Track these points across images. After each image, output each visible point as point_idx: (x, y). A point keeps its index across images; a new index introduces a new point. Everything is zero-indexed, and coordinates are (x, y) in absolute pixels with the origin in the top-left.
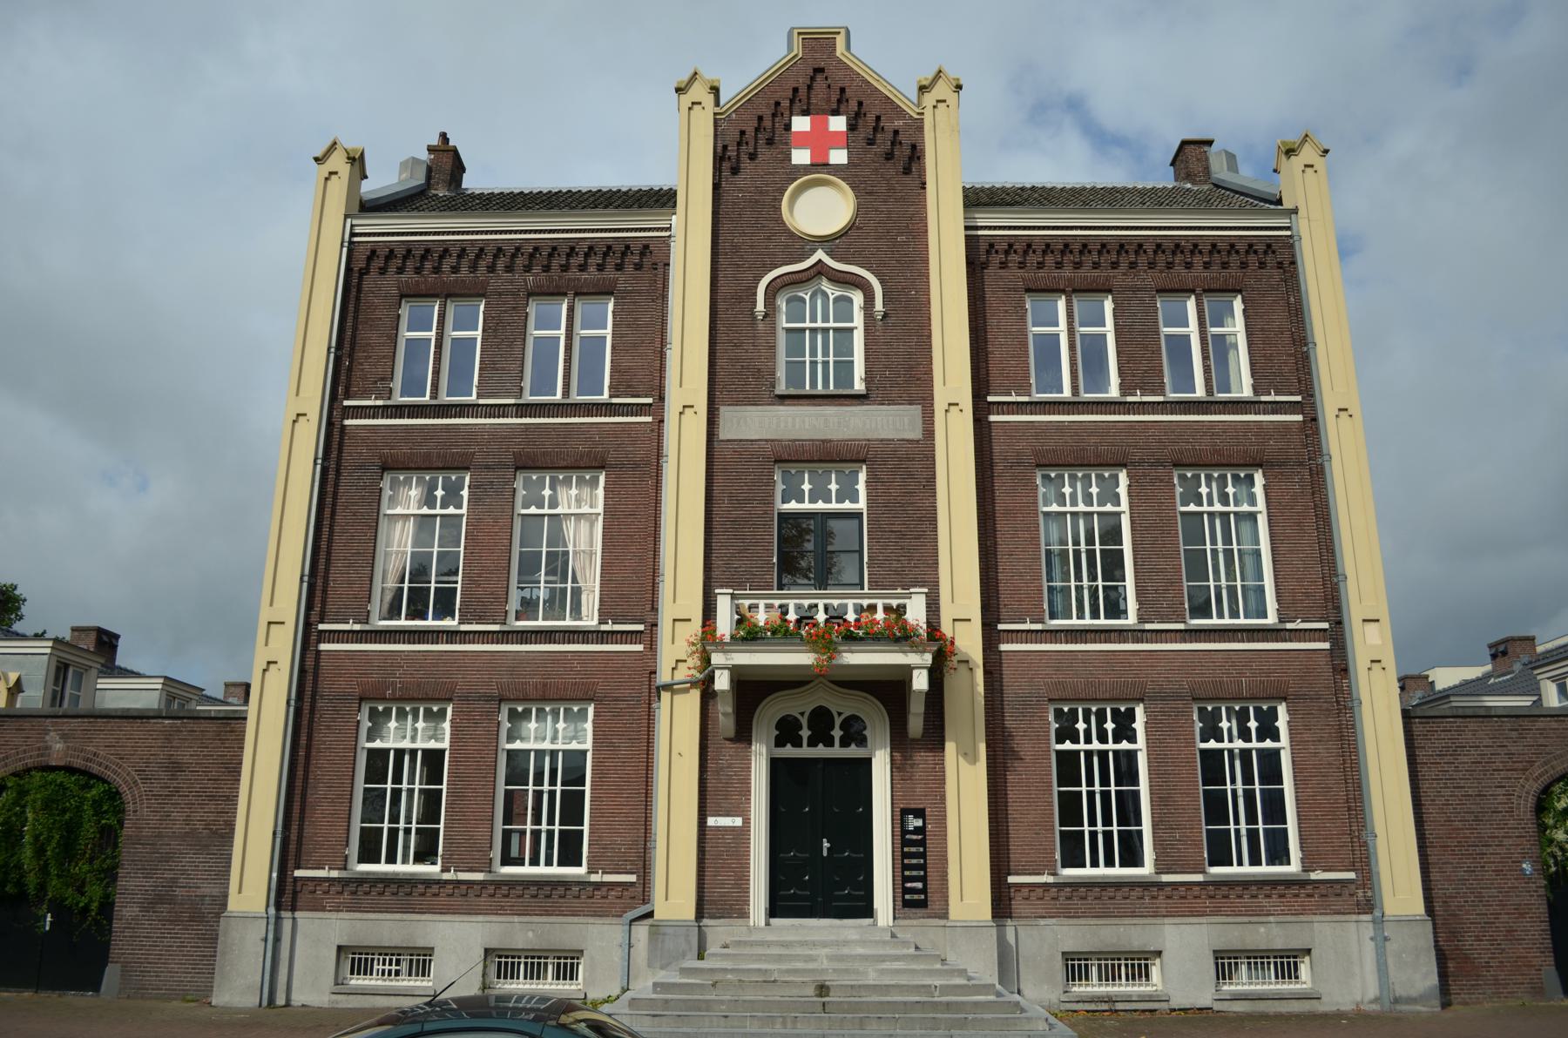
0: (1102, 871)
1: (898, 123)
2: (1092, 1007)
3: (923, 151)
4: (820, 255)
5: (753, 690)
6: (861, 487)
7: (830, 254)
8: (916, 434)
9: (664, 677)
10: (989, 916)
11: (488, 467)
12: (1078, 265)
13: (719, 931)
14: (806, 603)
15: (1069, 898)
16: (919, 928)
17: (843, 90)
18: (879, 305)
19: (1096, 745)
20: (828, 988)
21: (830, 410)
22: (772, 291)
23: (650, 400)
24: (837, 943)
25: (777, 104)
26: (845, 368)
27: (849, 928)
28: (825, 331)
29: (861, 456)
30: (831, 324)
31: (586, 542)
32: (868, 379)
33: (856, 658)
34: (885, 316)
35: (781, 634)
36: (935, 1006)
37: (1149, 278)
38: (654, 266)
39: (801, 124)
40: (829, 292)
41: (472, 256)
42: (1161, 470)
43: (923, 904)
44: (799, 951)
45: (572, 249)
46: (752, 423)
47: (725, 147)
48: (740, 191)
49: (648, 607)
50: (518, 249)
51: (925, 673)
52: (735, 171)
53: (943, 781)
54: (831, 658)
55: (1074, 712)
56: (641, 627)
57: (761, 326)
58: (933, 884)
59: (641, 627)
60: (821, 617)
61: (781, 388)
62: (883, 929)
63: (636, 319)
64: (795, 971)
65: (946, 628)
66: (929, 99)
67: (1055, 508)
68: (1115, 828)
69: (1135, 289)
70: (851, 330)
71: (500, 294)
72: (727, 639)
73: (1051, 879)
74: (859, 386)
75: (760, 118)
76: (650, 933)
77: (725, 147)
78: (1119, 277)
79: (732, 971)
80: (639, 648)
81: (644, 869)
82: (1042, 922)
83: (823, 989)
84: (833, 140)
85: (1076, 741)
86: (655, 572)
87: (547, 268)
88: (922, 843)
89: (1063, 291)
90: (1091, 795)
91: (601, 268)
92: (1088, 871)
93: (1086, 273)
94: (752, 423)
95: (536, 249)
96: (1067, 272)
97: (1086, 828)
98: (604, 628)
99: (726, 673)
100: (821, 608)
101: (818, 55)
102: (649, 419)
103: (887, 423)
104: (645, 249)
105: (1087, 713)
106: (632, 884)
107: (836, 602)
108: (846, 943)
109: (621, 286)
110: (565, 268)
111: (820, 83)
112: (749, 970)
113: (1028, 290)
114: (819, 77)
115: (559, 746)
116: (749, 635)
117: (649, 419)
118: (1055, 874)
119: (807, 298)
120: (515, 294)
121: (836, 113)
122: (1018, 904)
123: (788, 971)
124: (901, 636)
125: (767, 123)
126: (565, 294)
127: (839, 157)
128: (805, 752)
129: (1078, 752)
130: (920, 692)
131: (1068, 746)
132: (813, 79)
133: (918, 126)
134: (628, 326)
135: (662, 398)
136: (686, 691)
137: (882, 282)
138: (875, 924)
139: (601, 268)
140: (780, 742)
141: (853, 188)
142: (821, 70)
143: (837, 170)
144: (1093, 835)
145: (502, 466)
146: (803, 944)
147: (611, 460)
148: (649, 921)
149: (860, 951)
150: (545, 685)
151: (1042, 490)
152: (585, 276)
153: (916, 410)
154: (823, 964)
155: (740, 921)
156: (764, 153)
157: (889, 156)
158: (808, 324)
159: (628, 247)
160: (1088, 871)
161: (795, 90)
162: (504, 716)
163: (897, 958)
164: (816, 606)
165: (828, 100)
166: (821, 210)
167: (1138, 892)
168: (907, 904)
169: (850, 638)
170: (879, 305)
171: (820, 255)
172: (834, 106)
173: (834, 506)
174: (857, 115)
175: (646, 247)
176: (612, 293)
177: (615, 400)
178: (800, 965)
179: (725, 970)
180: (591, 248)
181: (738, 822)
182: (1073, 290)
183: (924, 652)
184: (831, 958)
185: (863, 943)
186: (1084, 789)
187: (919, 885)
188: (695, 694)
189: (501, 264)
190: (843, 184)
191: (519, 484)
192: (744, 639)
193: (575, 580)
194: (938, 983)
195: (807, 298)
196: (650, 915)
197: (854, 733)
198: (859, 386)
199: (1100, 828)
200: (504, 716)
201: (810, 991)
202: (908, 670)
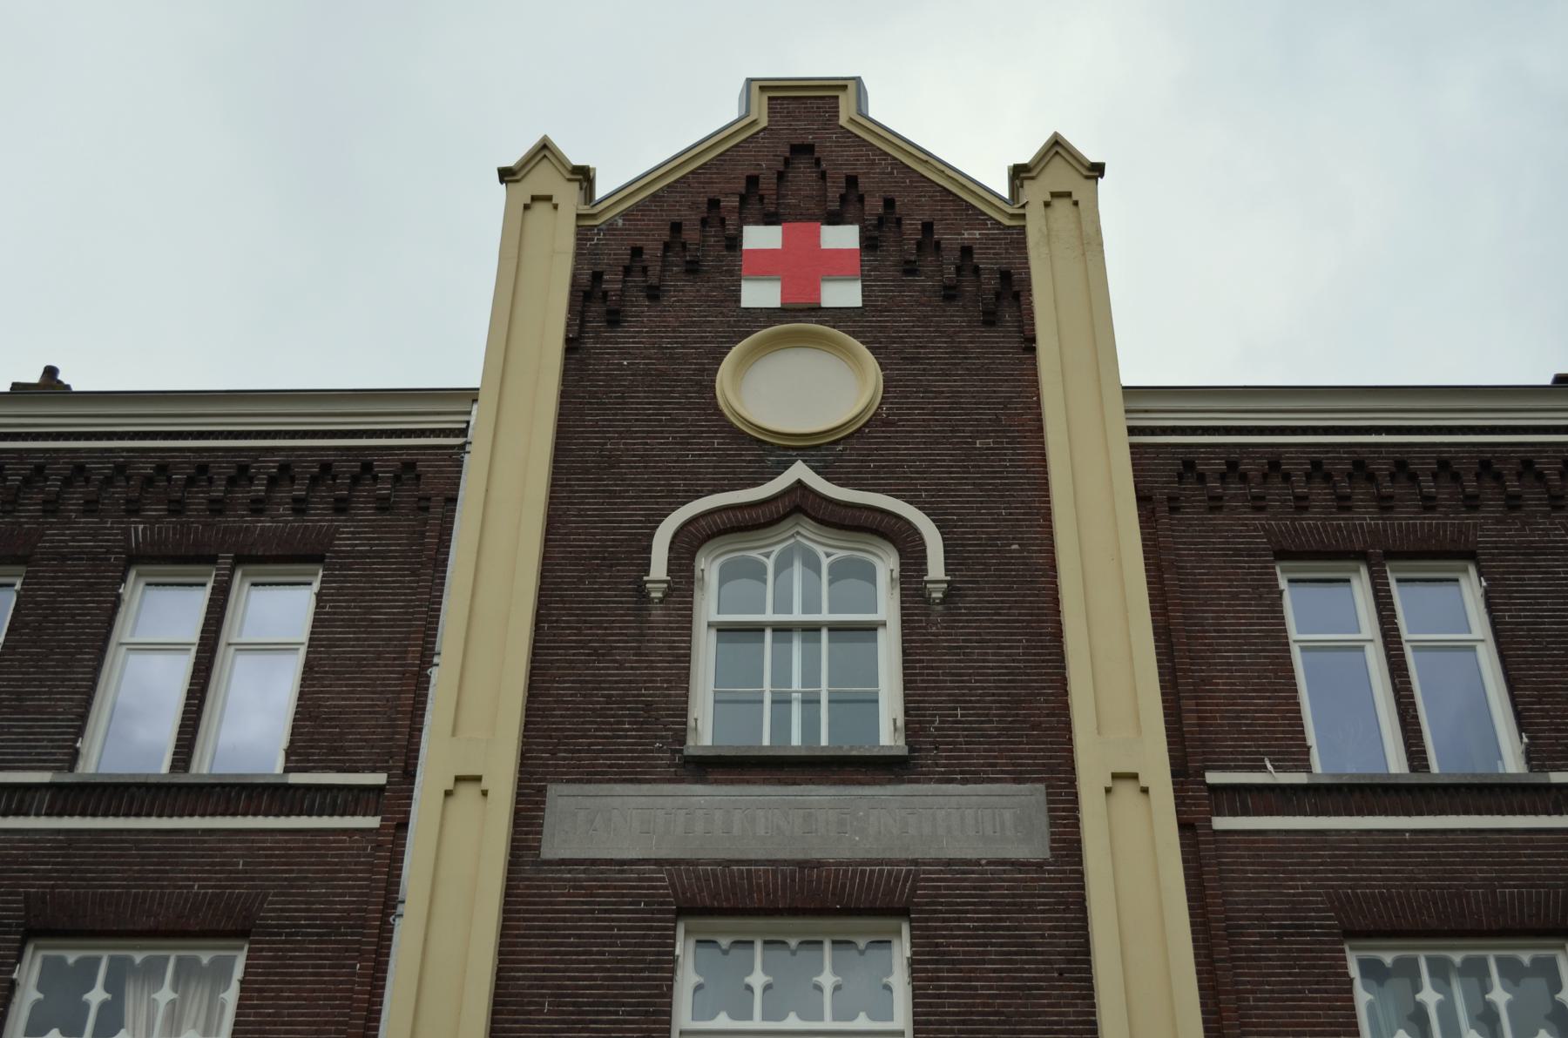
1: (971, 235)
3: (1027, 283)
4: (799, 471)
8: (1035, 847)
17: (852, 181)
18: (936, 567)
21: (820, 795)
22: (687, 544)
23: (380, 779)
28: (811, 629)
30: (825, 616)
32: (914, 722)
34: (951, 593)
39: (760, 238)
40: (820, 551)
47: (597, 277)
48: (625, 353)
52: (614, 319)
53: (427, 656)
57: (657, 614)
61: (704, 734)
66: (1034, 193)
70: (871, 629)
74: (888, 736)
89: (1362, 556)
102: (373, 822)
104: (408, 468)
109: (343, 543)
110: (217, 507)
111: (803, 173)
113: (1283, 555)
114: (802, 165)
117: (373, 822)
119: (770, 564)
121: (835, 219)
126: (211, 560)
133: (1017, 239)
137: (941, 526)
139: (300, 507)
141: (873, 351)
142: (808, 149)
143: (839, 317)
151: (1362, 997)
153: (1032, 796)
157: (950, 294)
158: (769, 616)
161: (752, 181)
165: (823, 198)
170: (936, 567)
171: (799, 471)
175: (409, 466)
176: (317, 559)
191: (29, 975)
195: (770, 564)
198: (888, 736)
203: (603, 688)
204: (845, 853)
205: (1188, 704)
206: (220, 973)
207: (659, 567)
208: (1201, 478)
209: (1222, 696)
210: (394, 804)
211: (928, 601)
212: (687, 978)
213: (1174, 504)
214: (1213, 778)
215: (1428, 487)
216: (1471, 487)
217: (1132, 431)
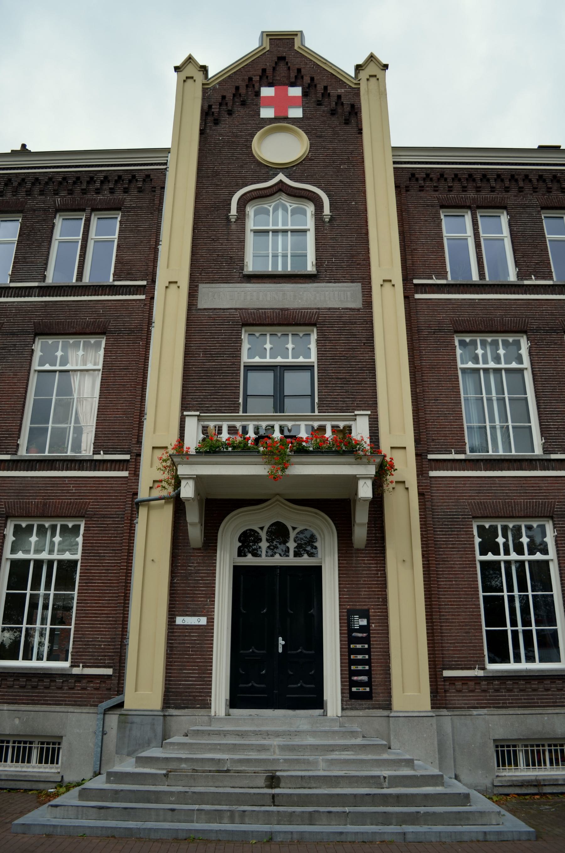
0: (524, 666)
1: (341, 91)
2: (524, 791)
4: (281, 177)
5: (218, 505)
6: (313, 347)
7: (289, 177)
8: (357, 304)
9: (143, 494)
10: (428, 707)
11: (13, 334)
12: (478, 190)
13: (184, 719)
14: (264, 424)
15: (497, 690)
16: (366, 719)
17: (299, 70)
19: (514, 556)
20: (278, 778)
21: (288, 287)
23: (144, 283)
24: (289, 734)
25: (250, 79)
26: (301, 257)
27: (301, 719)
29: (313, 321)
31: (87, 394)
33: (304, 469)
34: (332, 219)
35: (241, 450)
36: (386, 799)
37: (534, 199)
38: (153, 190)
39: (267, 92)
40: (288, 204)
41: (15, 184)
42: (554, 335)
43: (367, 696)
44: (254, 741)
45: (92, 178)
46: (223, 296)
47: (210, 107)
48: (221, 135)
49: (134, 441)
50: (50, 179)
51: (369, 483)
52: (216, 122)
54: (283, 469)
55: (494, 529)
56: (127, 457)
57: (233, 227)
58: (377, 678)
59: (127, 457)
60: (277, 435)
62: (332, 720)
63: (137, 226)
64: (248, 761)
65: (385, 448)
66: (363, 75)
67: (470, 365)
68: (534, 628)
69: (525, 207)
70: (305, 231)
71: (34, 210)
72: (192, 451)
73: (480, 673)
74: (310, 268)
75: (237, 88)
76: (119, 722)
77: (210, 107)
78: (511, 198)
79: (186, 760)
80: (125, 474)
81: (119, 662)
82: (475, 712)
83: (273, 781)
84: (293, 102)
85: (497, 553)
86: (142, 413)
87: (71, 192)
88: (367, 640)
89: (469, 207)
90: (511, 599)
91: (112, 191)
92: (511, 666)
93: (485, 195)
94: (223, 296)
95: (64, 179)
96: (471, 194)
97: (509, 628)
98: (97, 457)
99: (191, 483)
100: (277, 429)
101: (281, 49)
102: (143, 297)
103: (336, 296)
104: (148, 177)
105: (505, 529)
106: (109, 676)
107: (290, 424)
108: (297, 733)
109: (127, 204)
112: (202, 760)
113: (443, 207)
115: (55, 556)
116: (211, 449)
117: (143, 297)
118: (484, 669)
119: (271, 209)
120: (45, 210)
121: (293, 85)
122: (452, 696)
123: (241, 761)
124: (345, 447)
125: (243, 91)
126: (84, 210)
127: (296, 113)
128: (264, 560)
129: (499, 562)
130: (365, 500)
131: (490, 557)
132: (276, 63)
133: (356, 92)
134: (131, 231)
135: (154, 281)
136: (161, 507)
137: (329, 196)
138: (325, 714)
139: (112, 191)
140: (241, 553)
141: (306, 133)
143: (294, 121)
144: (515, 634)
145: (24, 332)
146: (256, 733)
147: (111, 327)
148: (118, 712)
149: (311, 741)
150: (45, 504)
151: (459, 352)
152: (101, 197)
153: (357, 287)
154: (275, 753)
155: (203, 712)
156: (240, 111)
157: (333, 113)
159: (134, 177)
160: (511, 666)
161: (264, 70)
162: (9, 531)
163: (346, 748)
164: (273, 427)
165: (289, 77)
166: (281, 148)
167: (535, 684)
168: (354, 696)
169: (301, 451)
171: (281, 177)
172: (293, 80)
173: (290, 360)
174: (309, 86)
175: (148, 176)
177: (117, 283)
178: (254, 755)
179: (180, 760)
180: (106, 178)
181: (203, 621)
182: (474, 207)
183: (369, 463)
184: (284, 748)
185: (314, 733)
186: (505, 594)
187: (365, 678)
188: (168, 512)
189: (36, 190)
190: (300, 131)
192: (206, 452)
193: (77, 420)
194: (386, 773)
195: (271, 209)
196: (121, 705)
197: (307, 545)
198: (310, 268)
199: (520, 628)
200: (9, 531)
201: (261, 782)
202: (354, 480)
203: (216, 254)
204: (295, 306)
205: (409, 257)
206: (98, 345)
207: (234, 211)
208: (417, 180)
209: (419, 252)
210: (149, 290)
211: (324, 222)
212: (245, 346)
213: (407, 189)
214: (416, 281)
215: (493, 183)
216: (507, 183)
217: (394, 163)
